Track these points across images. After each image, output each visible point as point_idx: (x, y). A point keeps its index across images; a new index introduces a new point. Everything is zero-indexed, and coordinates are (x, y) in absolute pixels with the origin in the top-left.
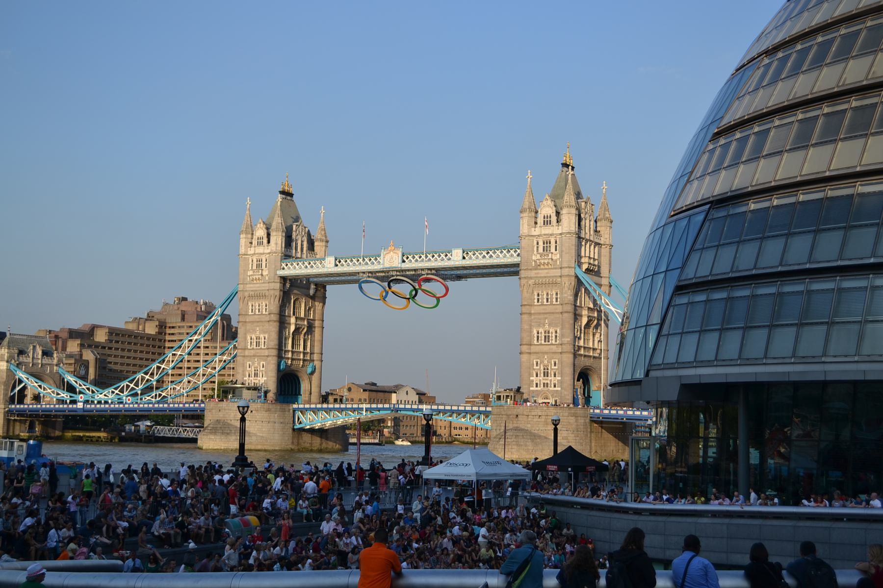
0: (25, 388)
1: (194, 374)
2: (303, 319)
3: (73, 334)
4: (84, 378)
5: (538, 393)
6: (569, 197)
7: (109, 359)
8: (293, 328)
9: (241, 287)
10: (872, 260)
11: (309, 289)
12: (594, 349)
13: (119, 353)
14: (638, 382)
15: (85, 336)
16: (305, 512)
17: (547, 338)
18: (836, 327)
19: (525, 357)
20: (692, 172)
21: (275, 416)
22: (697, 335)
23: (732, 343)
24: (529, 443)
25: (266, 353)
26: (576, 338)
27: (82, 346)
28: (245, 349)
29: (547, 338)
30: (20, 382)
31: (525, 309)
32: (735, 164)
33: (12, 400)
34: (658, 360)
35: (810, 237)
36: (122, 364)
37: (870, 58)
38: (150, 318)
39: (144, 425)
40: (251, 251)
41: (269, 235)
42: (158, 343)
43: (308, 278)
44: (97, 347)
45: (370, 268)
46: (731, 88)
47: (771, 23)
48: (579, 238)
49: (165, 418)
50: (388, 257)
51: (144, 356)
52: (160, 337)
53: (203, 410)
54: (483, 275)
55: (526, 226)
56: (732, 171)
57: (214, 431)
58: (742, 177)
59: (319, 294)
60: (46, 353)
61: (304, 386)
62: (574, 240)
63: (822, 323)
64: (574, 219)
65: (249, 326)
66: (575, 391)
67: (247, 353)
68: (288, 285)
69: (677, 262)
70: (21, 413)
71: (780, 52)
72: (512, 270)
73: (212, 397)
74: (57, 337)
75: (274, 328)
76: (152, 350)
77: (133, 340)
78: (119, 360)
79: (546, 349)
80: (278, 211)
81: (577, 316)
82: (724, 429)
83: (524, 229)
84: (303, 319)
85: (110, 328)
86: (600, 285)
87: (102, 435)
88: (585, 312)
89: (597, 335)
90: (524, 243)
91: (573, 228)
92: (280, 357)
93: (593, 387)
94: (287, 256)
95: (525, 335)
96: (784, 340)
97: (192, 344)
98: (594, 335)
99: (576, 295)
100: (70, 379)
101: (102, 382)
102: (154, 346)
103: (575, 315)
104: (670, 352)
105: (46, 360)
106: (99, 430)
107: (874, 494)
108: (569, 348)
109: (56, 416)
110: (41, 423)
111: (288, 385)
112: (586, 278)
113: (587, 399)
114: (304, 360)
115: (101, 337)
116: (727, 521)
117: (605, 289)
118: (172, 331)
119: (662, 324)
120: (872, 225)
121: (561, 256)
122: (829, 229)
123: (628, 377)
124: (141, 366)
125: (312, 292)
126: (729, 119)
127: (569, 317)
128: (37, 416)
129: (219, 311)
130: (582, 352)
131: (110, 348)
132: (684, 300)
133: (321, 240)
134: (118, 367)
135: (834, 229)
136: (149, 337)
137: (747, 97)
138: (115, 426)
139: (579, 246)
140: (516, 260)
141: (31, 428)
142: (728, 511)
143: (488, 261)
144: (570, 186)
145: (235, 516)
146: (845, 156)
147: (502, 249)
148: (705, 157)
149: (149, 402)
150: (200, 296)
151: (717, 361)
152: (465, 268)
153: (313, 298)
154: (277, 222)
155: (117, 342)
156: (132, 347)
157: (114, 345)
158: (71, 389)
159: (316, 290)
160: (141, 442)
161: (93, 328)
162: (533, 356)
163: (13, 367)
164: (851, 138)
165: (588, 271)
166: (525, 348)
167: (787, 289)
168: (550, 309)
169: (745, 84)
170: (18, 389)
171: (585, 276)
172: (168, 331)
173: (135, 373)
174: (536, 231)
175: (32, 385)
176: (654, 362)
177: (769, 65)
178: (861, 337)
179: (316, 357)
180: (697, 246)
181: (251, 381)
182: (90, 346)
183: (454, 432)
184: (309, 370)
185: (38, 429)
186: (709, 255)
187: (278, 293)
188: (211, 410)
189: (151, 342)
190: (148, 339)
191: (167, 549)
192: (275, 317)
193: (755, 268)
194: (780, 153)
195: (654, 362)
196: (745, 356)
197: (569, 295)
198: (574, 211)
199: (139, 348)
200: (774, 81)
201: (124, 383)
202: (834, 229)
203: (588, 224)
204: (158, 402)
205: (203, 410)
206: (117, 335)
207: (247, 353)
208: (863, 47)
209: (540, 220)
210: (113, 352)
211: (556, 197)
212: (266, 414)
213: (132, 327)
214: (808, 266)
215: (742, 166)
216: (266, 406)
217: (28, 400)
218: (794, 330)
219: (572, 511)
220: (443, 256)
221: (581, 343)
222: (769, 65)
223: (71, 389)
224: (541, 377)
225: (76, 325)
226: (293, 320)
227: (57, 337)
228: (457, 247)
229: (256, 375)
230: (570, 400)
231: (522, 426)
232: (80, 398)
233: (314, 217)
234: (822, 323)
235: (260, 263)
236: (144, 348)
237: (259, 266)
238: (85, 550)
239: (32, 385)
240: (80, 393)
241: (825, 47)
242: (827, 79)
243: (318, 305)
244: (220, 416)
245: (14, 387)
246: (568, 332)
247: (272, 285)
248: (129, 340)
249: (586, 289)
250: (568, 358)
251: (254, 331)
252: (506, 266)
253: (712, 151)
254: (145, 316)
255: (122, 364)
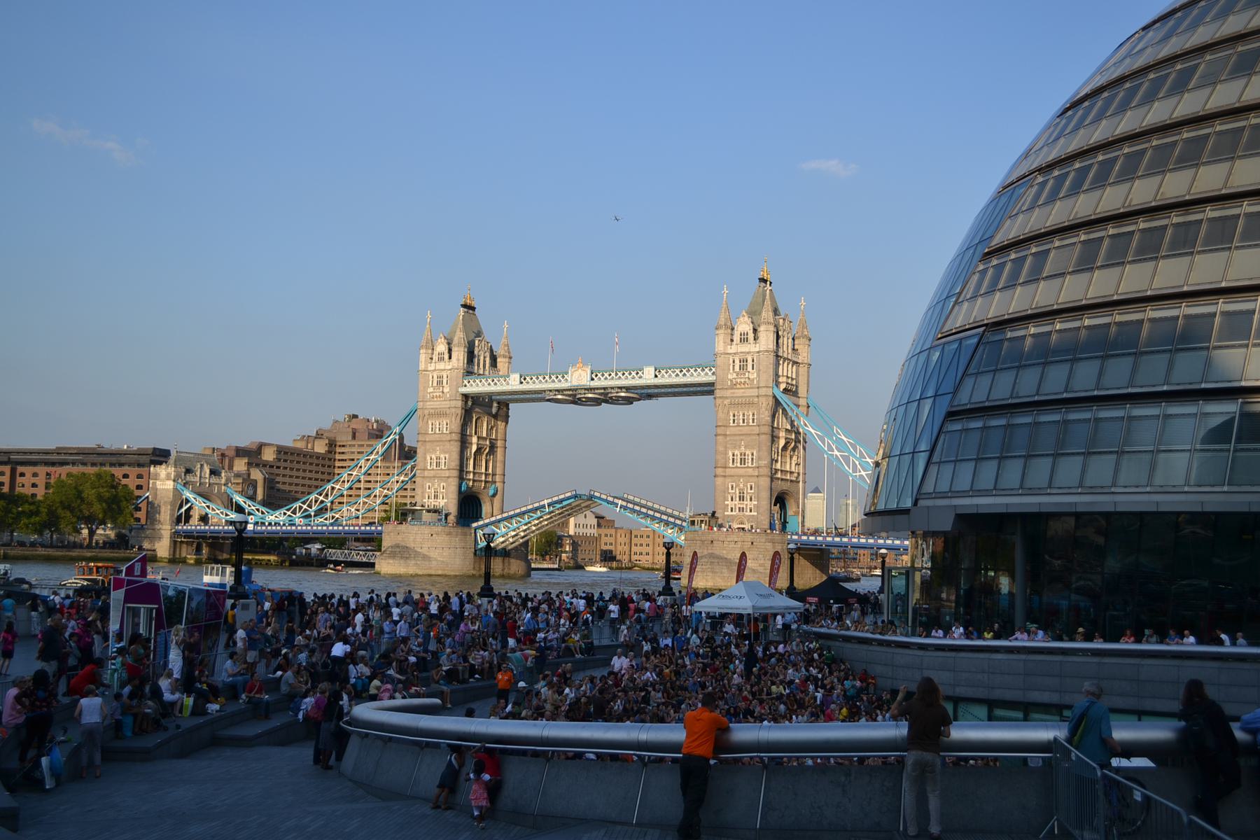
0: (190, 508)
1: (369, 496)
2: (485, 439)
3: (240, 452)
4: (252, 498)
5: (733, 518)
6: (767, 314)
7: (278, 479)
8: (474, 448)
9: (420, 405)
10: (1165, 388)
11: (491, 407)
12: (791, 473)
13: (288, 472)
14: (906, 512)
15: (252, 454)
16: (577, 645)
17: (743, 461)
18: (1126, 456)
19: (719, 481)
20: (960, 293)
21: (457, 541)
22: (973, 463)
23: (988, 471)
24: (725, 571)
25: (447, 474)
26: (774, 461)
27: (249, 464)
28: (424, 469)
29: (743, 461)
30: (187, 501)
31: (720, 431)
32: (1011, 286)
33: (178, 520)
34: (929, 487)
35: (1097, 363)
36: (290, 484)
37: (1158, 178)
38: (319, 436)
39: (315, 548)
40: (431, 367)
41: (450, 351)
42: (328, 463)
43: (490, 396)
44: (264, 466)
45: (558, 385)
46: (1000, 205)
47: (1038, 139)
48: (777, 356)
49: (338, 541)
50: (576, 374)
51: (319, 476)
52: (330, 456)
53: (380, 533)
54: (675, 394)
55: (721, 343)
56: (1008, 293)
57: (393, 555)
58: (1017, 301)
59: (502, 413)
60: (213, 472)
61: (486, 508)
62: (772, 357)
63: (1111, 452)
64: (772, 337)
65: (428, 446)
66: (772, 516)
67: (426, 473)
68: (470, 403)
69: (948, 386)
70: (188, 535)
71: (1053, 171)
72: (707, 389)
73: (389, 519)
74: (223, 455)
75: (455, 447)
76: (322, 469)
77: (302, 459)
78: (287, 480)
79: (741, 472)
80: (460, 326)
81: (774, 438)
82: (994, 563)
83: (720, 346)
84: (485, 439)
85: (278, 446)
86: (798, 406)
87: (272, 558)
88: (782, 434)
89: (795, 458)
90: (719, 361)
91: (772, 346)
92: (461, 479)
93: (790, 512)
94: (469, 373)
95: (719, 457)
96: (1069, 469)
97: (369, 464)
98: (791, 457)
99: (773, 416)
100: (239, 499)
101: (274, 500)
102: (323, 466)
103: (773, 436)
104: (941, 479)
105: (214, 480)
106: (268, 553)
107: (1186, 632)
108: (766, 471)
109: (223, 538)
110: (209, 545)
111: (469, 506)
112: (783, 399)
113: (784, 524)
114: (486, 482)
115: (269, 455)
116: (1023, 657)
117: (803, 409)
118: (342, 450)
119: (932, 451)
120: (1164, 351)
121: (758, 375)
122: (1118, 355)
123: (893, 506)
124: (317, 487)
125: (494, 410)
126: (999, 239)
127: (766, 439)
128: (204, 538)
129: (397, 430)
130: (779, 475)
131: (278, 467)
132: (957, 426)
133: (504, 357)
134: (287, 488)
135: (1123, 355)
136: (318, 456)
137: (1021, 217)
138: (286, 549)
139: (777, 365)
140: (711, 379)
141: (198, 550)
142: (1024, 647)
143: (681, 380)
144: (768, 302)
145: (513, 651)
146: (1134, 278)
147: (696, 367)
148: (976, 277)
149: (321, 524)
150: (372, 413)
151: (996, 490)
152: (656, 387)
153: (495, 417)
154: (459, 337)
155: (285, 461)
156: (302, 466)
157: (282, 464)
158: (240, 509)
159: (499, 408)
160: (312, 565)
161: (261, 446)
162: (728, 480)
163: (179, 487)
164: (1140, 261)
165: (786, 391)
166: (719, 471)
167: (1073, 416)
168: (746, 430)
169: (1018, 200)
170: (185, 508)
171: (784, 396)
172: (338, 450)
173: (309, 493)
174: (732, 349)
175: (199, 505)
176: (924, 491)
177: (1044, 183)
178: (1153, 467)
179: (498, 478)
180: (971, 371)
181: (431, 503)
182: (257, 465)
183: (634, 558)
184: (491, 492)
185: (205, 551)
186: (985, 381)
187: (459, 411)
188: (389, 533)
189: (321, 462)
190: (318, 458)
191: (455, 685)
192: (456, 437)
193: (1037, 394)
194: (1062, 275)
195: (924, 491)
196: (1028, 484)
197: (766, 416)
198: (772, 328)
199: (308, 467)
200: (1052, 198)
201: (297, 504)
202: (1123, 355)
203: (786, 342)
204: (332, 525)
205: (380, 533)
206: (286, 453)
207: (426, 473)
208: (1148, 167)
209: (737, 338)
210: (281, 471)
211: (753, 313)
212: (447, 538)
213: (300, 445)
214: (1096, 393)
215: (1019, 289)
216: (447, 529)
217: (195, 520)
218: (1050, 459)
219: (849, 645)
220: (634, 374)
221: (778, 466)
222: (1044, 183)
223: (240, 509)
224: (737, 502)
225: (244, 443)
226: (475, 439)
227: (223, 455)
228: (649, 365)
229: (436, 497)
230: (767, 526)
231: (717, 552)
232: (251, 519)
233: (498, 331)
234: (1111, 452)
235: (441, 379)
236: (314, 468)
237: (440, 383)
238: (389, 686)
239: (199, 505)
240: (250, 514)
241: (1107, 165)
242: (1111, 199)
243: (501, 425)
244: (399, 539)
245: (181, 507)
246: (765, 454)
247: (453, 403)
248: (297, 459)
249: (784, 410)
250: (765, 482)
251: (435, 451)
252: (700, 385)
253: (984, 272)
254: (314, 434)
255: (290, 484)
